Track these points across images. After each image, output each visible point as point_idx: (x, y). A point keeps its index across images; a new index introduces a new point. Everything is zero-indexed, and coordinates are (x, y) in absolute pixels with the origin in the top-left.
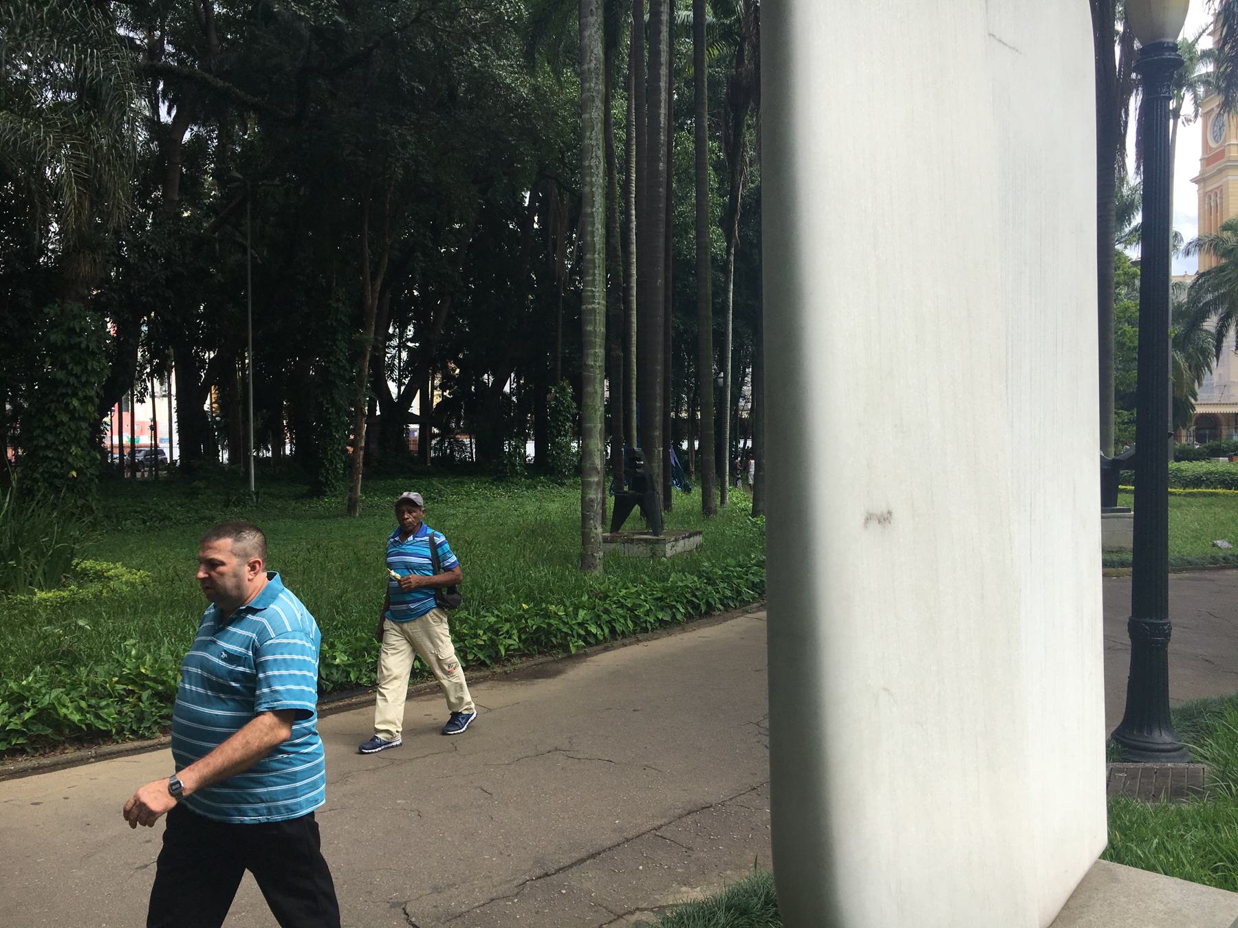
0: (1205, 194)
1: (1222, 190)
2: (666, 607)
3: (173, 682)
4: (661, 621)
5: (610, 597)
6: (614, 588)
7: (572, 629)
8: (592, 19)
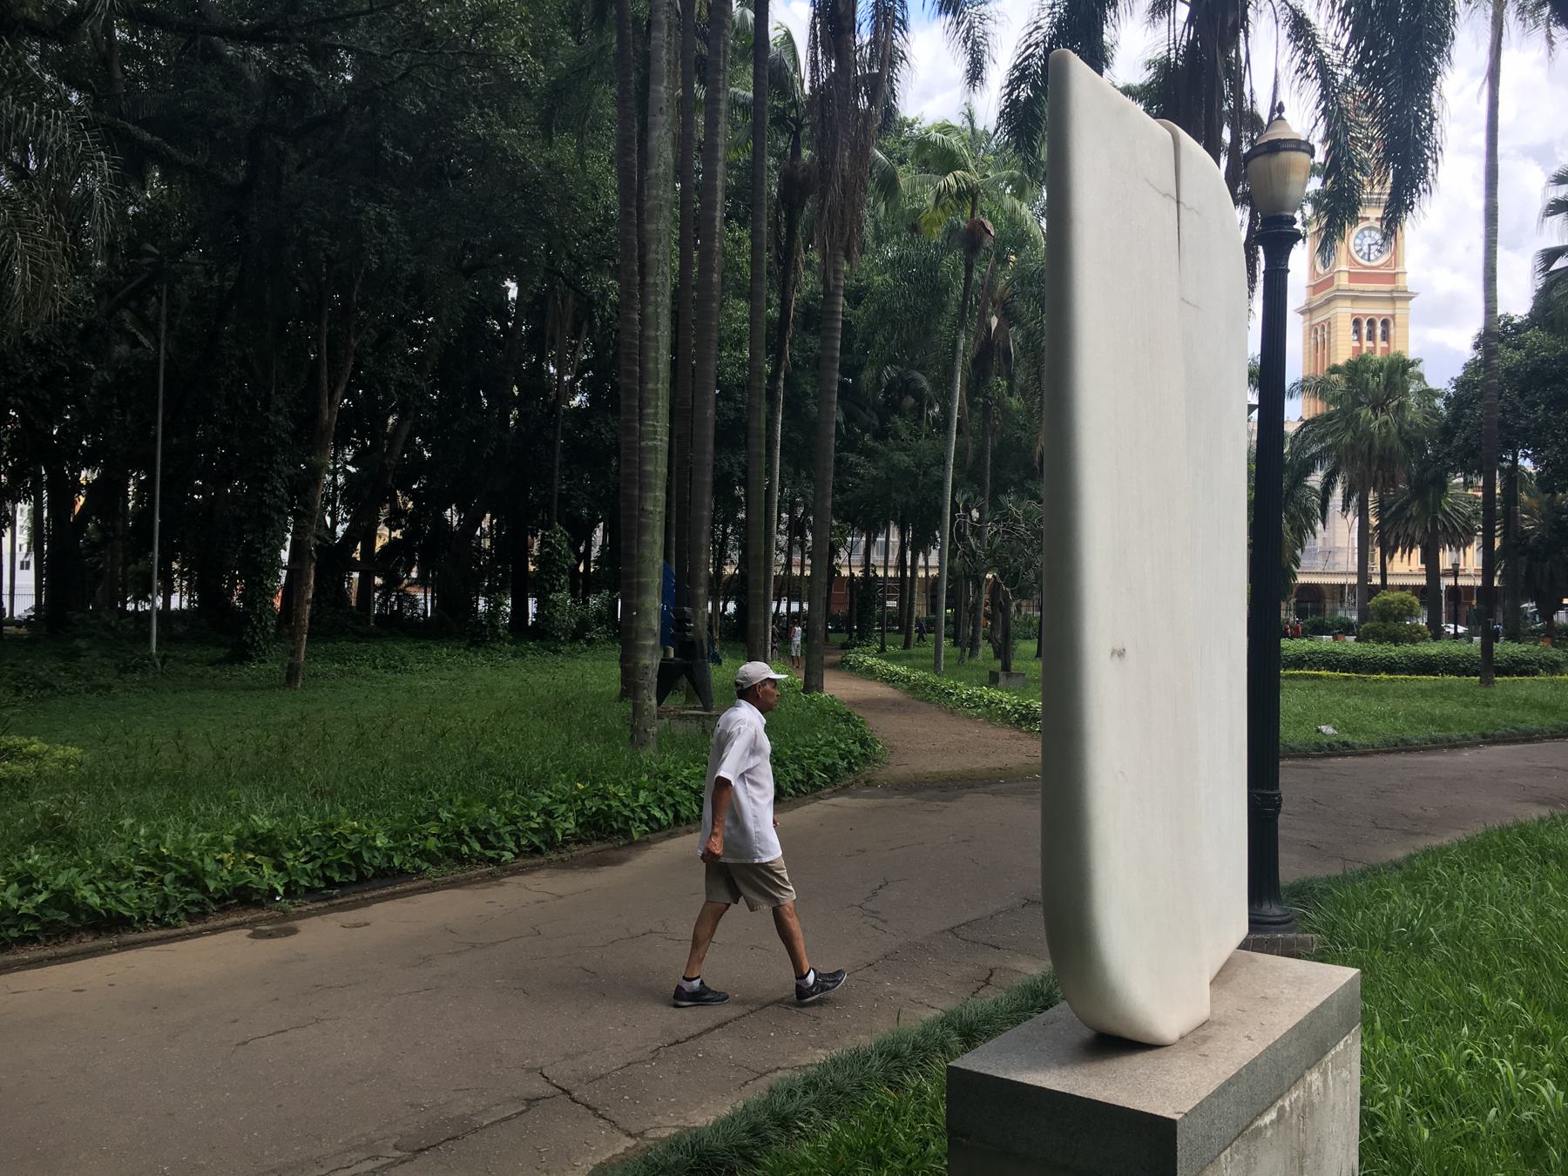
0: (1311, 326)
1: (1329, 324)
3: (199, 863)
6: (676, 768)
7: (633, 811)
8: (662, 119)
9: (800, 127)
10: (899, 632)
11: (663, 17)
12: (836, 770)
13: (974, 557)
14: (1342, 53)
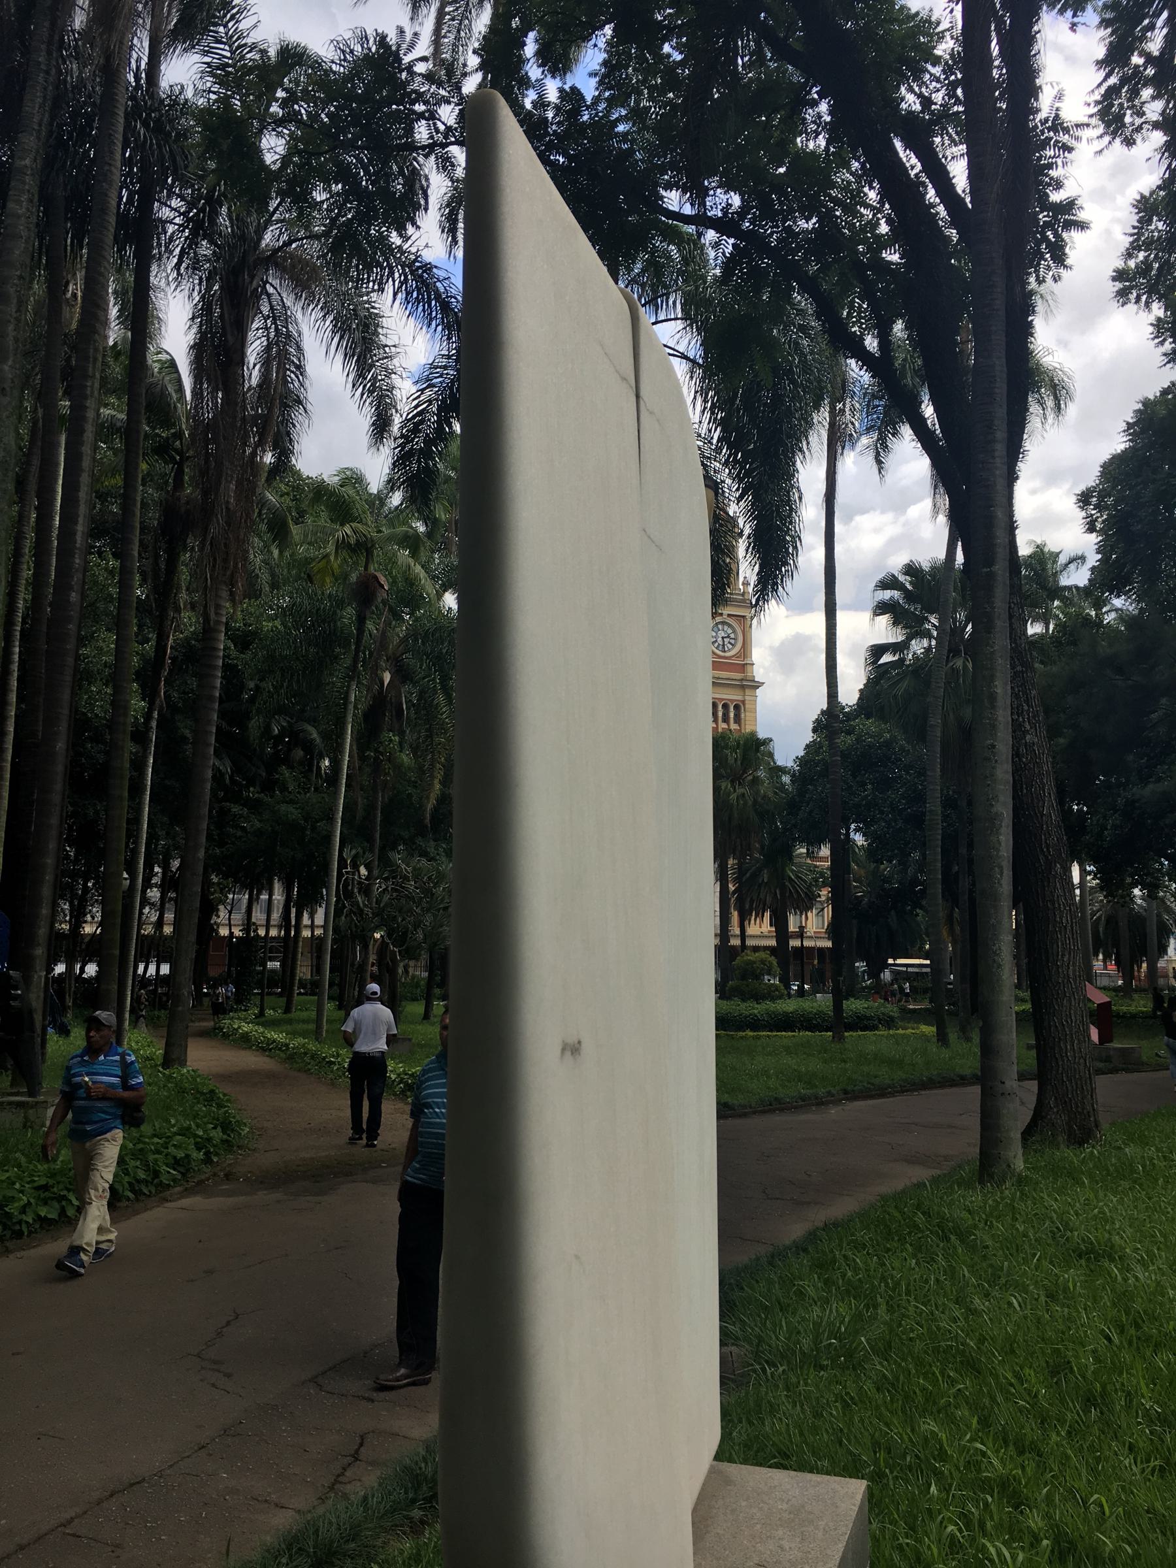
2: (53, 1199)
4: (44, 1221)
10: (280, 995)
12: (189, 1163)
13: (361, 915)
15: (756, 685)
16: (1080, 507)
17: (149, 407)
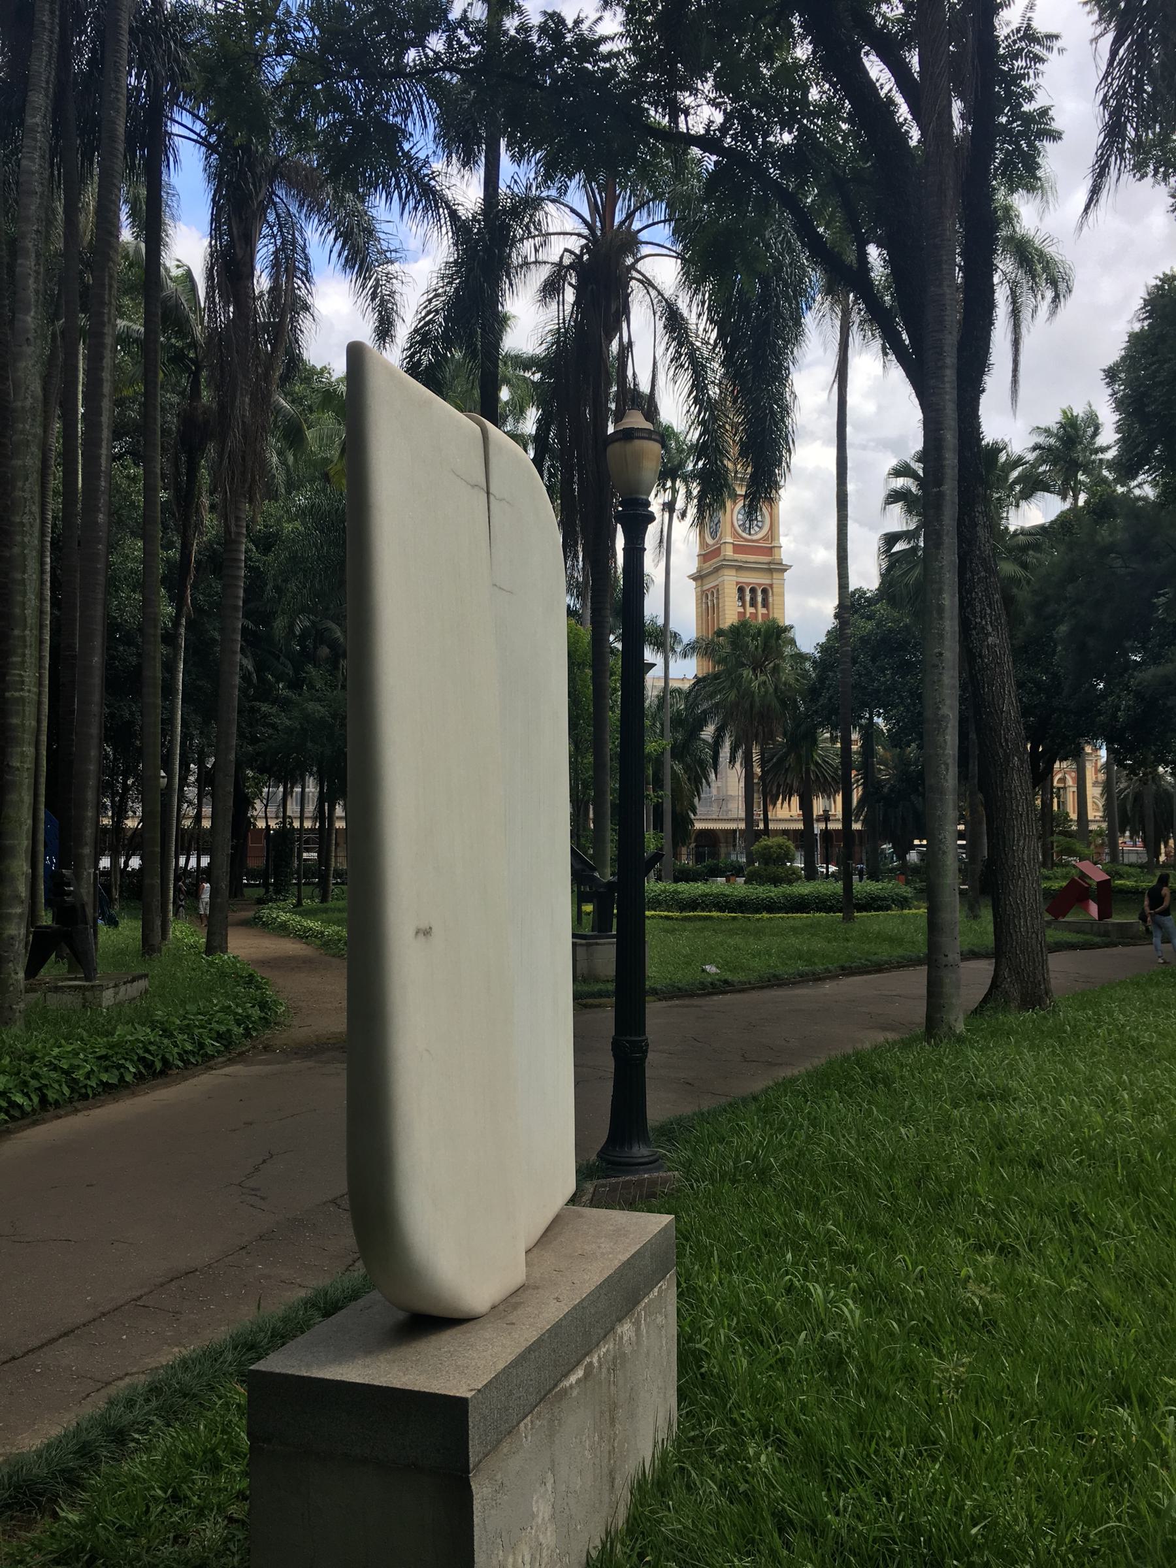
0: (703, 592)
1: (718, 590)
2: (113, 1067)
4: (107, 1087)
5: (38, 1058)
6: (44, 1047)
8: (29, 350)
9: (199, 369)
11: (30, 245)
12: (231, 1037)
14: (710, 347)
15: (783, 569)
16: (1107, 384)
17: (165, 317)
